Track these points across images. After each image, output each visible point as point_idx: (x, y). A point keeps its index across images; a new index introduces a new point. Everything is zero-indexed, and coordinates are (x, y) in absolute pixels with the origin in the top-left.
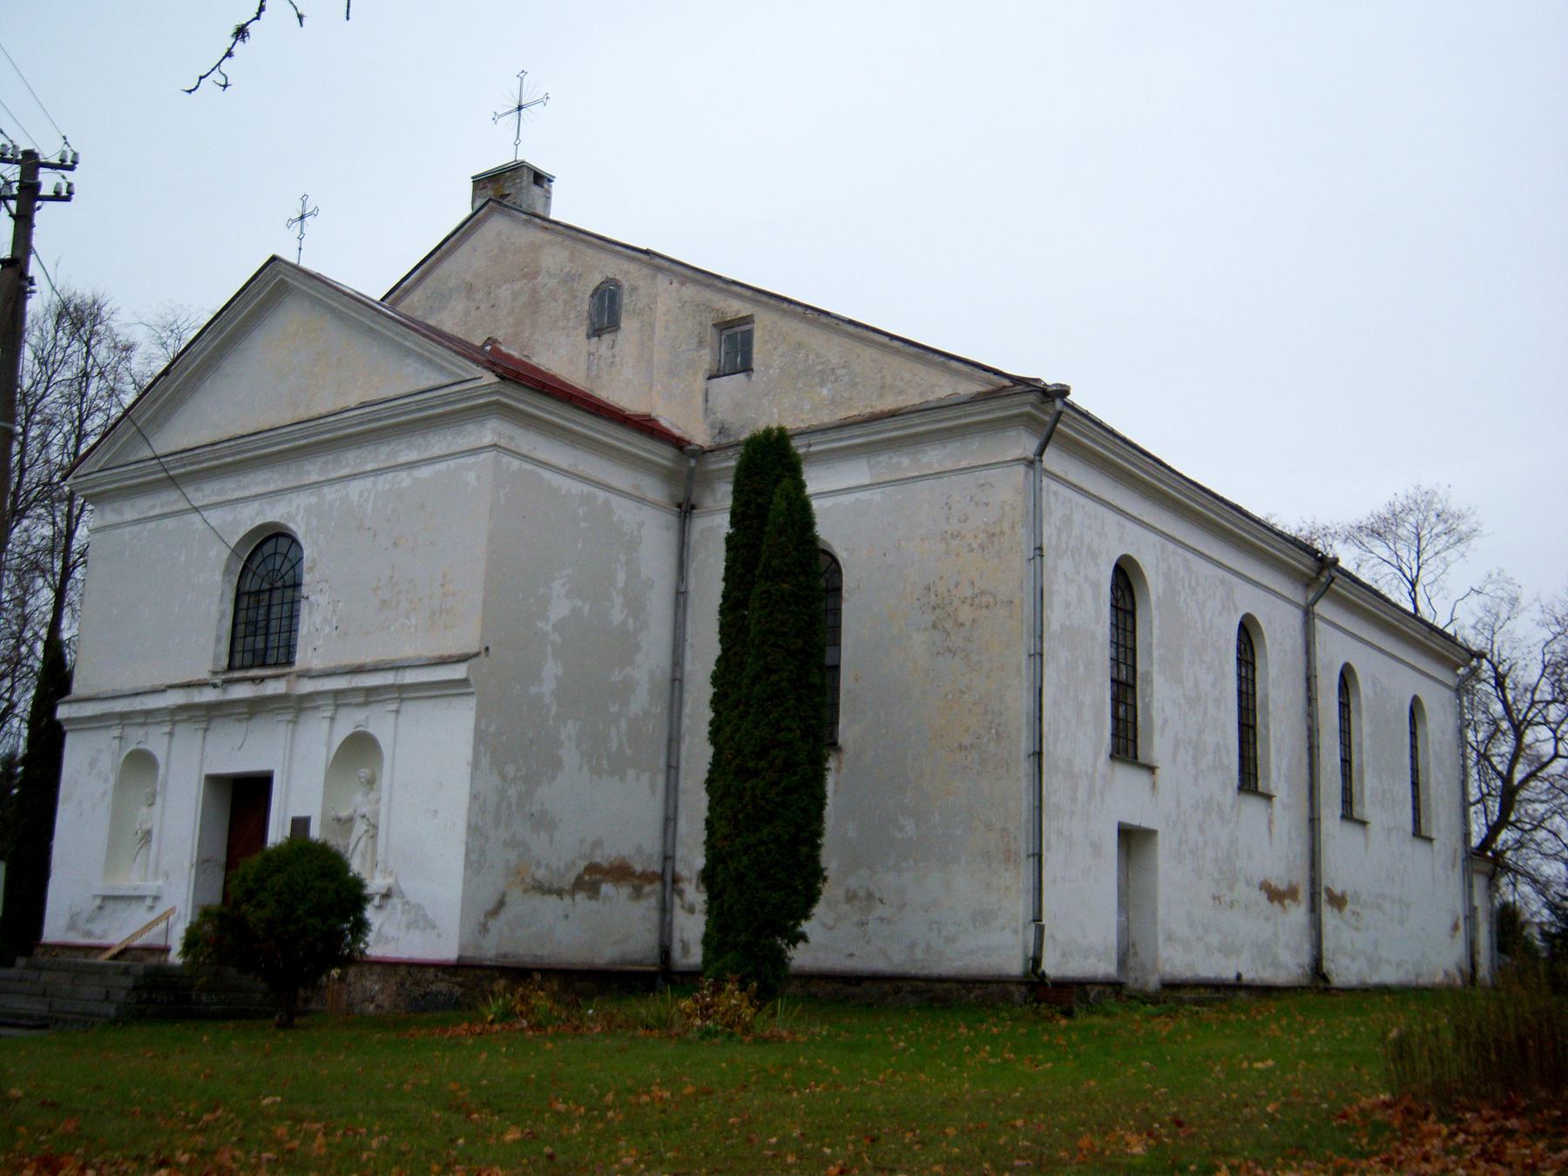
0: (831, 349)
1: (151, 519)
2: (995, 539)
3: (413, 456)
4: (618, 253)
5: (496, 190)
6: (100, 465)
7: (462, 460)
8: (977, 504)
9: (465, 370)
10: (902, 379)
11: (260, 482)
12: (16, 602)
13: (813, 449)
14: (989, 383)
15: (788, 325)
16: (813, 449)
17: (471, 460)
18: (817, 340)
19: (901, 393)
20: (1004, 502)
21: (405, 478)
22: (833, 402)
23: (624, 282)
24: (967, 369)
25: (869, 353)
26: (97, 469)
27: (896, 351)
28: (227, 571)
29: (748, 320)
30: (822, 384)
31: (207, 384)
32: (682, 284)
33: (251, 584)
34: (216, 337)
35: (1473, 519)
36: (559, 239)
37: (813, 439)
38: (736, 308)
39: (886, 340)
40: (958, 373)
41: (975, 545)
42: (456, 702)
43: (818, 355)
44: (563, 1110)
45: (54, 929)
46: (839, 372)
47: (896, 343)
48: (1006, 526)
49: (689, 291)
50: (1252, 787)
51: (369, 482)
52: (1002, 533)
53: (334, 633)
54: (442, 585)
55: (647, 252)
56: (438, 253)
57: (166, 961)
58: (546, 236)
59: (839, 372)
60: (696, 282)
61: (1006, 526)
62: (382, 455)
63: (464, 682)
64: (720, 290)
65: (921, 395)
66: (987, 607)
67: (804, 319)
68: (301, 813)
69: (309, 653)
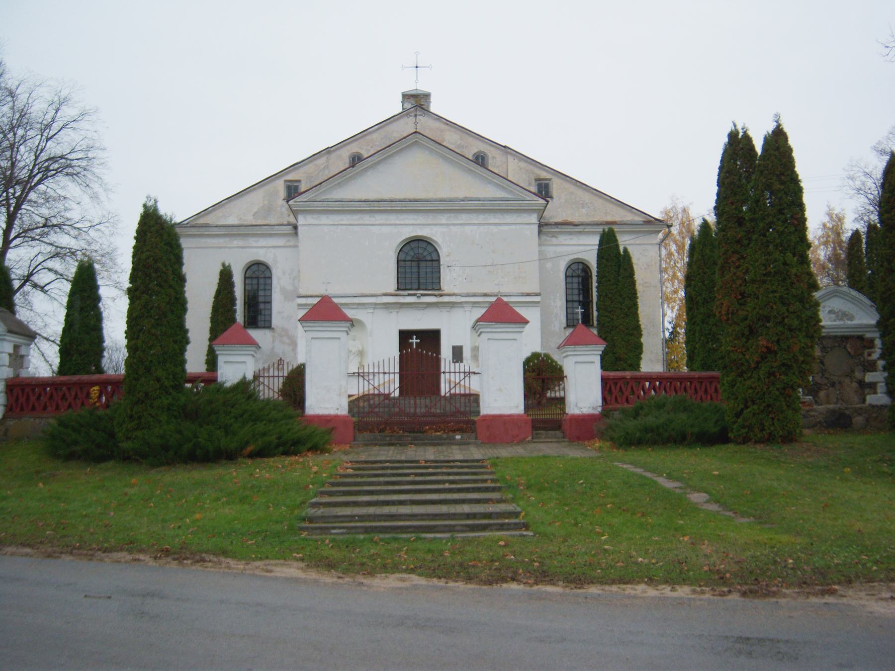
0: (586, 197)
1: (342, 225)
3: (497, 221)
4: (486, 143)
5: (416, 102)
6: (309, 198)
9: (528, 196)
12: (666, 306)
13: (585, 230)
14: (644, 217)
15: (567, 185)
16: (585, 230)
17: (528, 226)
18: (580, 193)
21: (494, 229)
23: (489, 154)
24: (639, 213)
25: (600, 201)
26: (306, 200)
27: (612, 203)
28: (395, 251)
29: (550, 180)
30: (583, 207)
31: (369, 173)
32: (520, 161)
33: (402, 257)
34: (379, 157)
36: (454, 130)
37: (587, 227)
38: (544, 175)
39: (609, 198)
40: (635, 213)
41: (643, 268)
42: (535, 308)
45: (444, 389)
47: (613, 200)
48: (653, 263)
49: (523, 164)
50: (591, 324)
51: (475, 227)
52: (652, 265)
53: (465, 281)
55: (505, 147)
56: (388, 121)
57: (29, 372)
58: (447, 127)
60: (525, 161)
61: (653, 263)
62: (481, 218)
63: (538, 302)
64: (539, 167)
67: (575, 185)
68: (458, 343)
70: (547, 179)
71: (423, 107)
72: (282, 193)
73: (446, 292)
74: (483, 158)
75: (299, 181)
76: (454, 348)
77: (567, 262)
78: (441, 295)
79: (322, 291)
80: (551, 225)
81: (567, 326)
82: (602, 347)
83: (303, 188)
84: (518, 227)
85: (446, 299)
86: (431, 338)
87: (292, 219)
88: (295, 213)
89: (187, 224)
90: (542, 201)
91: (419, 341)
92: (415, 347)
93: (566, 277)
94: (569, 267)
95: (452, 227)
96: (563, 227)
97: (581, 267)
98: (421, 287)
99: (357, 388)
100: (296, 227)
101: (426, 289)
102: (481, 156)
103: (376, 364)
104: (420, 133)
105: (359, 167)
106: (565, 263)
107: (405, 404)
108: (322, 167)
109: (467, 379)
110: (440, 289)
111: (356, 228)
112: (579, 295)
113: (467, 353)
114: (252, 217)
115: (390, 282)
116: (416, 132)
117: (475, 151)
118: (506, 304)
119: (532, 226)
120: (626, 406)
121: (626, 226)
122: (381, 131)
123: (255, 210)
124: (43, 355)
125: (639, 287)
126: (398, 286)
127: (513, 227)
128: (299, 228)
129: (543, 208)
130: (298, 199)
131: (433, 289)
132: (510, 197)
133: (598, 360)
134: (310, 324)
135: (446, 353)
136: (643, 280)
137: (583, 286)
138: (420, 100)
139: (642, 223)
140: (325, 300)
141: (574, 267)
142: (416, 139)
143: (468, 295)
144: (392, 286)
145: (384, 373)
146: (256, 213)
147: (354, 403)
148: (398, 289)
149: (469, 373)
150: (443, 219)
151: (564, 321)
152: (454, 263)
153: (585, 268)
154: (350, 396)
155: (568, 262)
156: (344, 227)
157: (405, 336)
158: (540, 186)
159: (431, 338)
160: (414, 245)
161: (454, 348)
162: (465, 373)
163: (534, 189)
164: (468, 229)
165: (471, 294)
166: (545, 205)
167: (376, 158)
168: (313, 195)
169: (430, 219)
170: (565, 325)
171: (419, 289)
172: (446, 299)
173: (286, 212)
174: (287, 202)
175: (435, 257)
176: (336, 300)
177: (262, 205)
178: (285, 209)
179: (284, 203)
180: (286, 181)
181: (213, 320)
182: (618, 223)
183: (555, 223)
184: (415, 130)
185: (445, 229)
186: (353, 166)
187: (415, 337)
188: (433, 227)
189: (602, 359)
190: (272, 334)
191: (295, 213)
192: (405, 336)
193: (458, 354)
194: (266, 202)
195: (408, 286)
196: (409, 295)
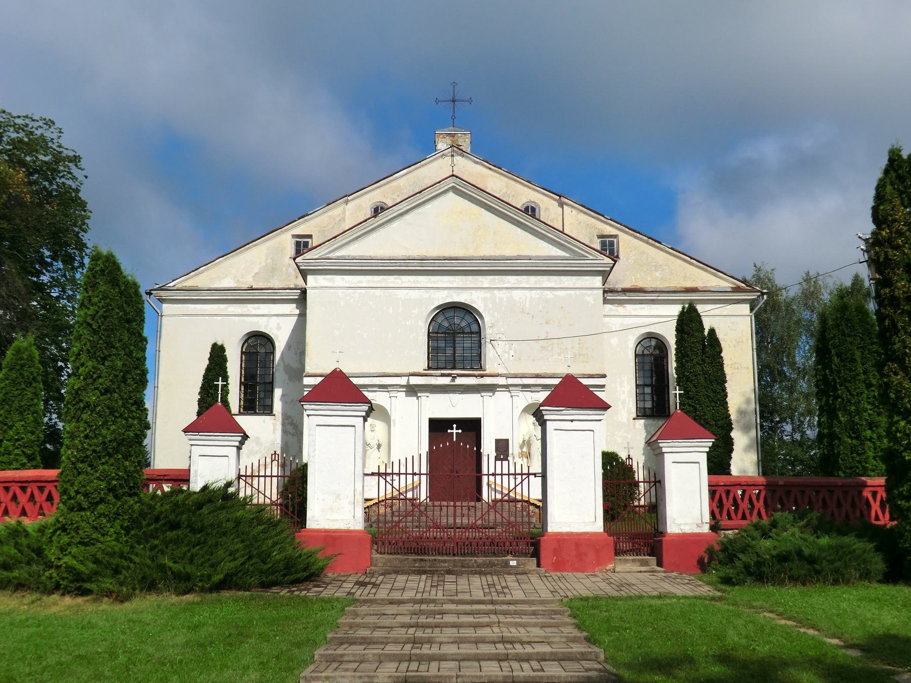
2: (740, 344)
7: (585, 291)
8: (731, 329)
10: (694, 275)
11: (458, 281)
17: (590, 292)
19: (694, 281)
20: (743, 330)
21: (549, 294)
22: (662, 279)
23: (541, 204)
29: (616, 236)
30: (656, 270)
35: (89, 214)
41: (731, 345)
43: (653, 259)
44: (515, 564)
46: (664, 267)
50: (667, 414)
52: (743, 342)
54: (579, 344)
59: (664, 267)
61: (744, 339)
65: (703, 283)
66: (738, 369)
69: (496, 366)
70: (611, 236)
71: (461, 147)
72: (291, 250)
73: (487, 372)
74: (533, 209)
75: (310, 236)
76: (498, 441)
77: (636, 337)
78: (482, 376)
79: (564, 370)
80: (617, 292)
81: (637, 416)
82: (708, 443)
83: (315, 242)
84: (578, 292)
85: (488, 381)
86: (472, 426)
87: (300, 282)
88: (304, 274)
89: (174, 286)
90: (608, 261)
91: (460, 431)
92: (455, 440)
93: (636, 355)
94: (639, 343)
95: (496, 292)
96: (632, 294)
97: (653, 343)
98: (457, 366)
99: (374, 490)
100: (304, 292)
101: (463, 369)
102: (531, 206)
103: (403, 462)
104: (457, 177)
105: (383, 217)
106: (635, 339)
107: (516, 517)
108: (338, 219)
109: (525, 482)
110: (481, 368)
111: (378, 292)
112: (652, 377)
113: (514, 449)
114: (251, 280)
115: (419, 359)
116: (453, 175)
117: (525, 200)
118: (586, 387)
119: (596, 292)
120: (744, 522)
121: (698, 294)
122: (410, 175)
123: (256, 271)
124: (190, 457)
125: (727, 369)
126: (428, 364)
127: (572, 292)
128: (308, 291)
129: (609, 269)
130: (308, 255)
131: (472, 369)
132: (567, 255)
133: (703, 459)
134: (313, 407)
135: (488, 448)
136: (731, 359)
137: (656, 366)
138: (457, 140)
139: (730, 290)
140: (570, 381)
141: (646, 343)
142: (453, 184)
143: (538, 376)
144: (421, 364)
145: (414, 474)
146: (257, 273)
147: (370, 509)
148: (429, 368)
149: (529, 474)
150: (485, 281)
151: (634, 410)
152: (498, 336)
153: (660, 344)
154: (366, 500)
155: (638, 338)
156: (363, 291)
157: (438, 426)
158: (603, 244)
159: (472, 426)
160: (450, 313)
161: (498, 441)
162: (522, 474)
163: (598, 247)
164: (517, 294)
165: (534, 376)
166: (612, 265)
167: (404, 207)
168: (326, 251)
169: (469, 281)
170: (634, 415)
171: (454, 368)
172: (403, 381)
173: (293, 273)
174: (294, 259)
175: (474, 328)
176: (355, 381)
177: (263, 264)
178: (293, 270)
179: (292, 262)
180: (294, 236)
181: (201, 402)
182: (700, 290)
183: (622, 289)
184: (451, 173)
185: (488, 295)
186: (375, 216)
187: (455, 426)
188: (473, 292)
189: (709, 459)
190: (273, 421)
191: (304, 274)
192: (438, 426)
193: (502, 448)
194: (269, 261)
195: (442, 365)
196: (443, 375)
